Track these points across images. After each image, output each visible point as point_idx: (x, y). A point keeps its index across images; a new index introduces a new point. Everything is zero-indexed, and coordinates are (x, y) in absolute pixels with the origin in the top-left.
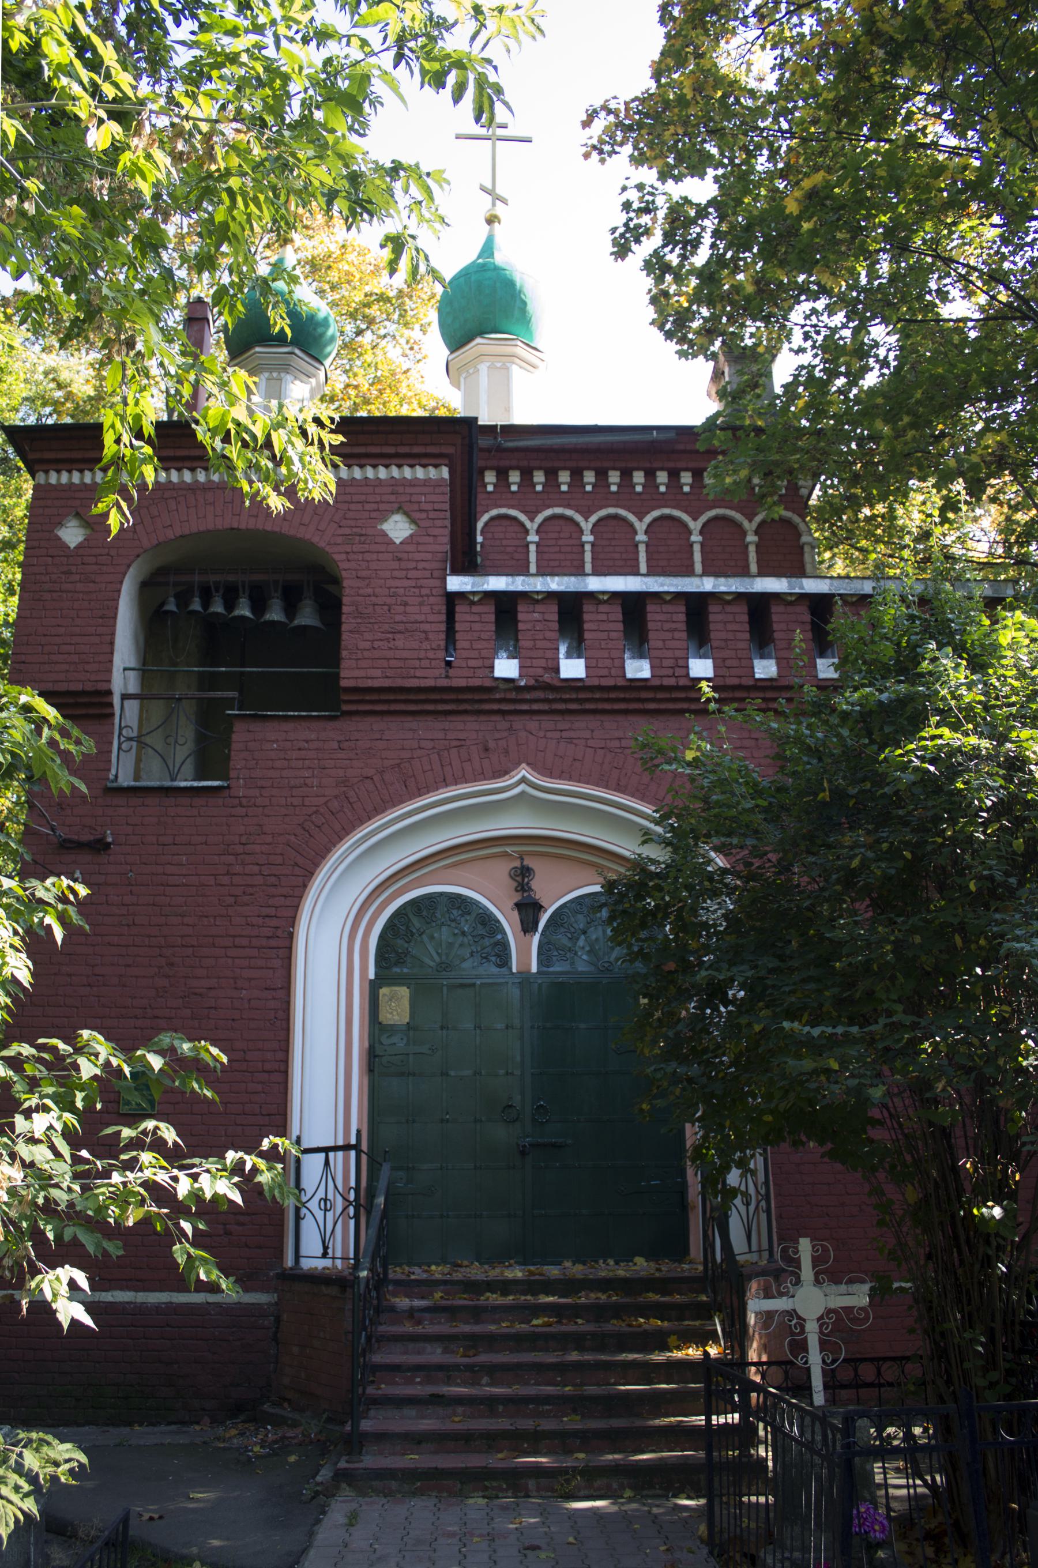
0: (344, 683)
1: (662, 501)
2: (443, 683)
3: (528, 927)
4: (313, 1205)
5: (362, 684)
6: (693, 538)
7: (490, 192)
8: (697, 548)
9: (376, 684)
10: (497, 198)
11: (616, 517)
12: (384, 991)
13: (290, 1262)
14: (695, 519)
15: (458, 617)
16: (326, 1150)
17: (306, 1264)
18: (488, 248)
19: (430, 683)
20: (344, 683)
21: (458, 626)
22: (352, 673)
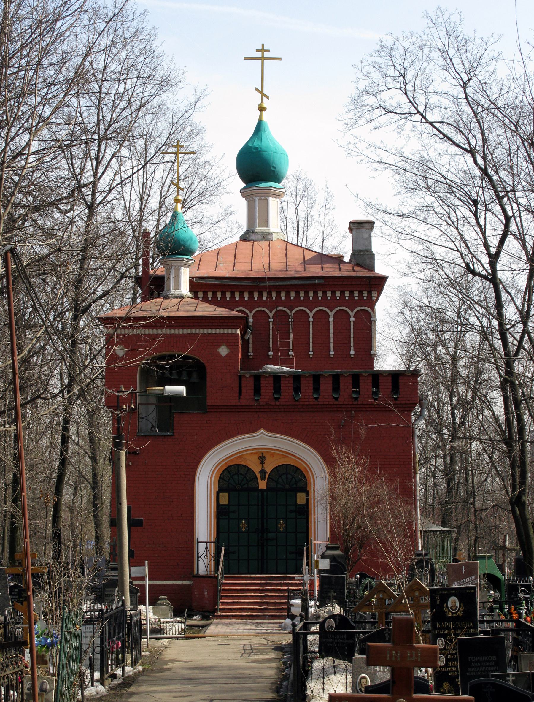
0: (208, 404)
1: (320, 304)
2: (238, 404)
3: (263, 478)
4: (203, 557)
5: (213, 404)
6: (330, 319)
7: (261, 92)
8: (331, 323)
9: (217, 404)
10: (263, 95)
11: (302, 310)
12: (221, 494)
13: (196, 573)
14: (331, 311)
15: (243, 382)
16: (207, 543)
17: (201, 573)
18: (259, 128)
19: (234, 404)
20: (208, 404)
21: (243, 385)
22: (210, 401)
